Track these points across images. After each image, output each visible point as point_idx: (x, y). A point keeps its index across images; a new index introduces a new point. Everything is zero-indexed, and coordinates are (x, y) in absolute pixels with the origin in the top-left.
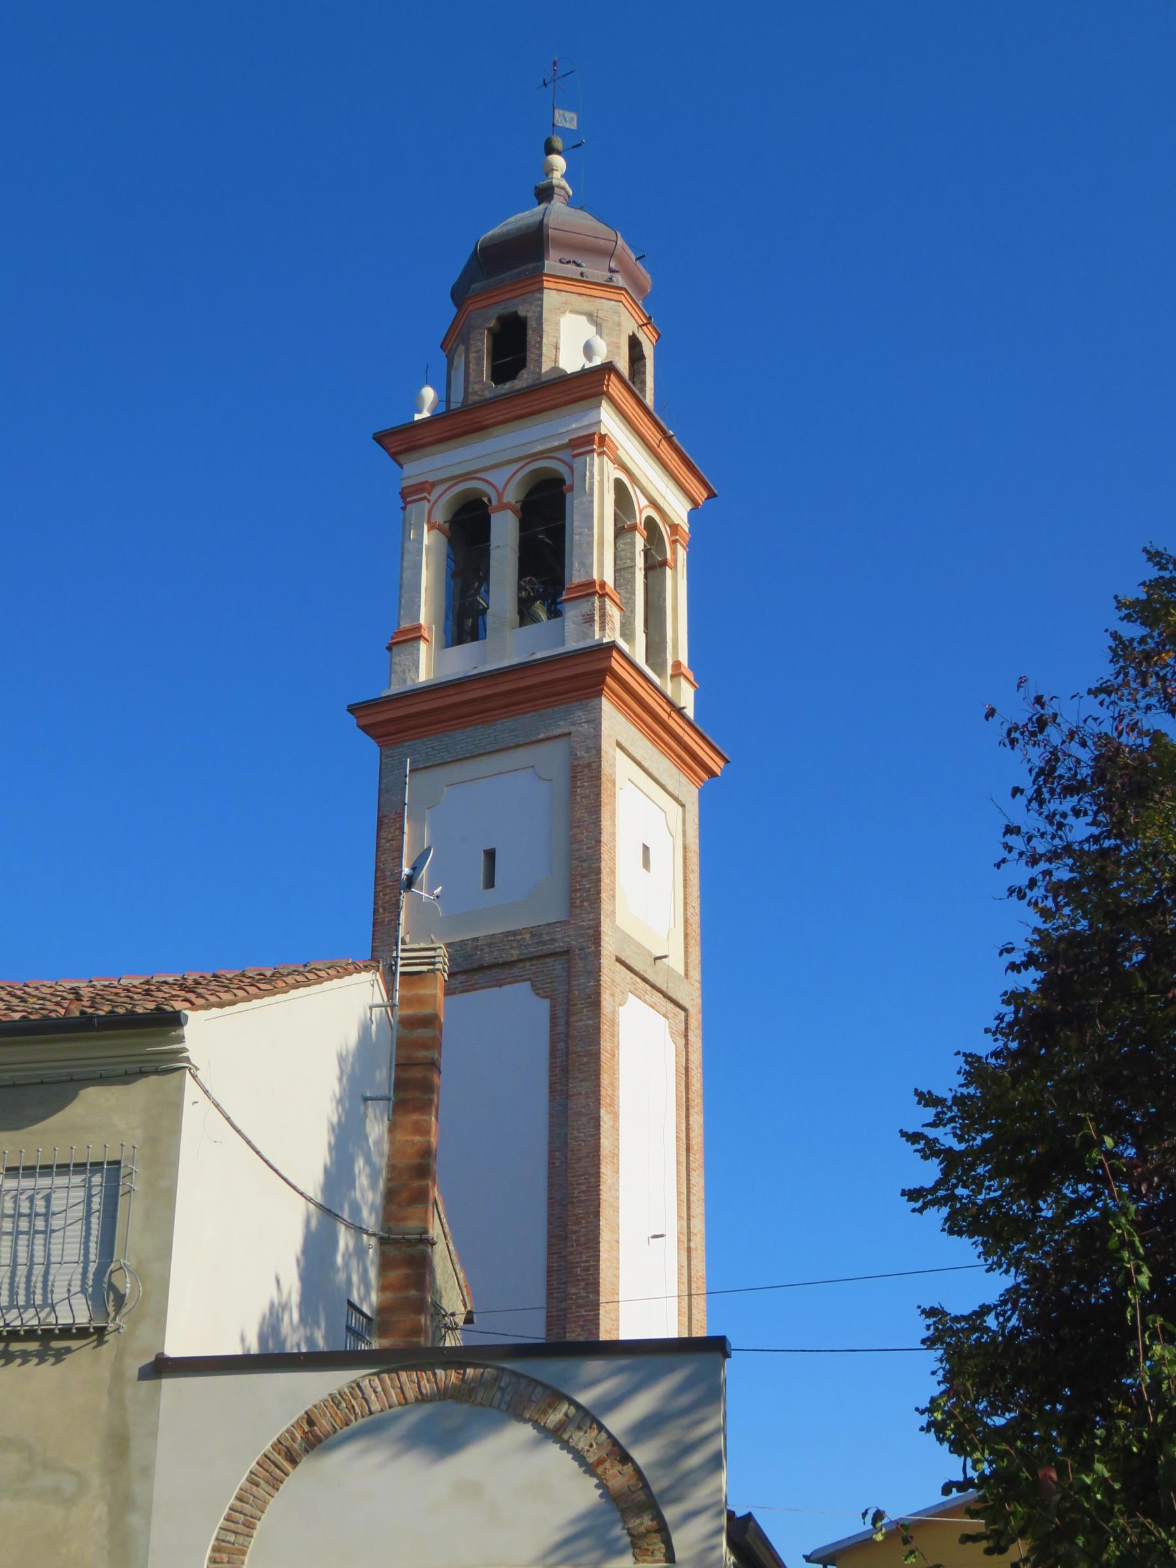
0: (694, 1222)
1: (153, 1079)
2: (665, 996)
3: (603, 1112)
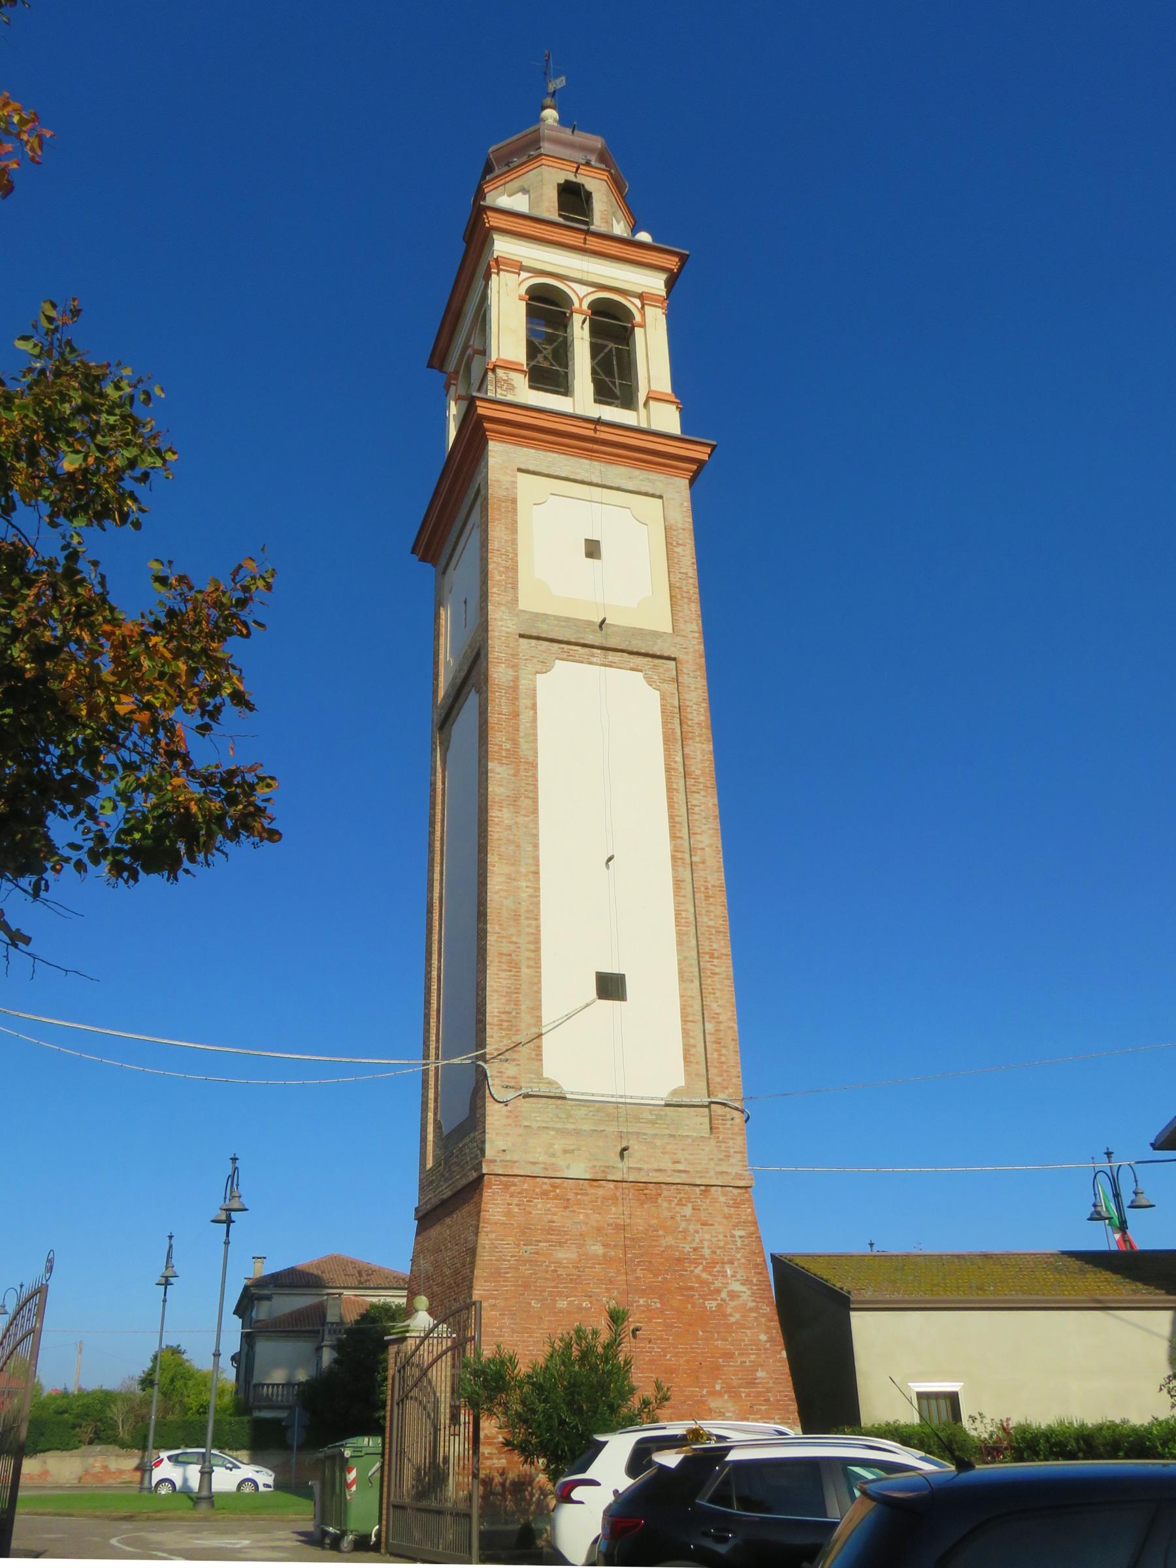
2: (631, 653)
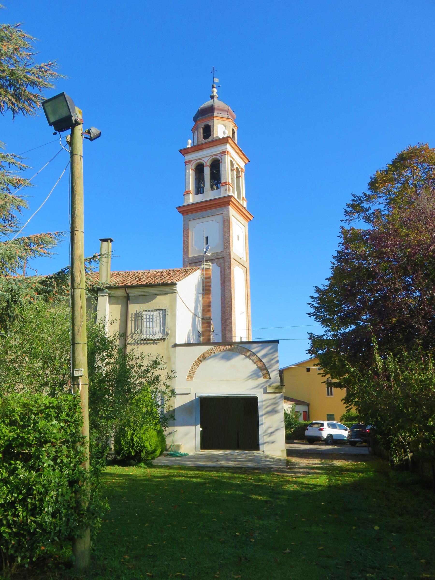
0: (249, 310)
1: (171, 294)
3: (232, 289)
